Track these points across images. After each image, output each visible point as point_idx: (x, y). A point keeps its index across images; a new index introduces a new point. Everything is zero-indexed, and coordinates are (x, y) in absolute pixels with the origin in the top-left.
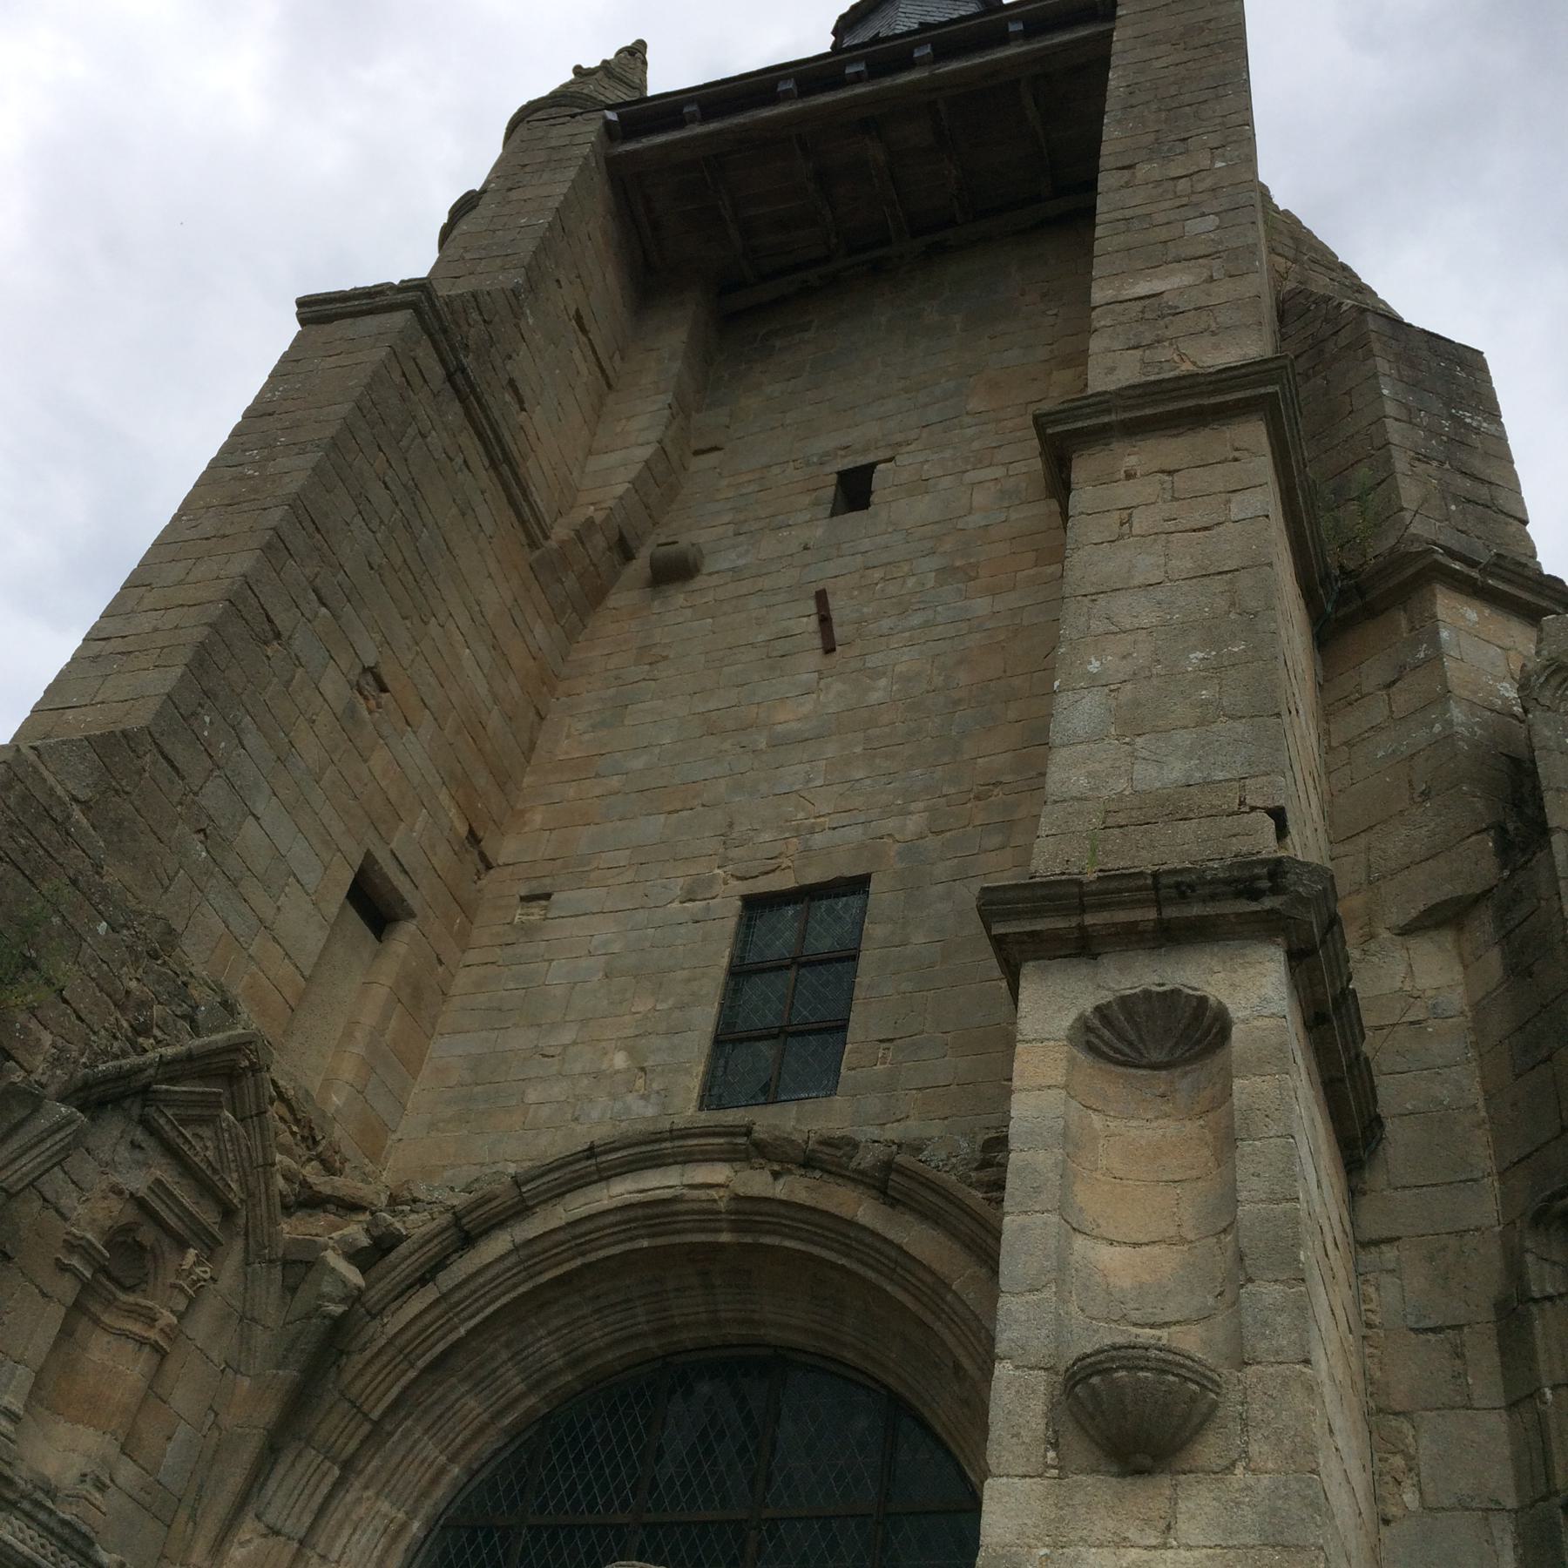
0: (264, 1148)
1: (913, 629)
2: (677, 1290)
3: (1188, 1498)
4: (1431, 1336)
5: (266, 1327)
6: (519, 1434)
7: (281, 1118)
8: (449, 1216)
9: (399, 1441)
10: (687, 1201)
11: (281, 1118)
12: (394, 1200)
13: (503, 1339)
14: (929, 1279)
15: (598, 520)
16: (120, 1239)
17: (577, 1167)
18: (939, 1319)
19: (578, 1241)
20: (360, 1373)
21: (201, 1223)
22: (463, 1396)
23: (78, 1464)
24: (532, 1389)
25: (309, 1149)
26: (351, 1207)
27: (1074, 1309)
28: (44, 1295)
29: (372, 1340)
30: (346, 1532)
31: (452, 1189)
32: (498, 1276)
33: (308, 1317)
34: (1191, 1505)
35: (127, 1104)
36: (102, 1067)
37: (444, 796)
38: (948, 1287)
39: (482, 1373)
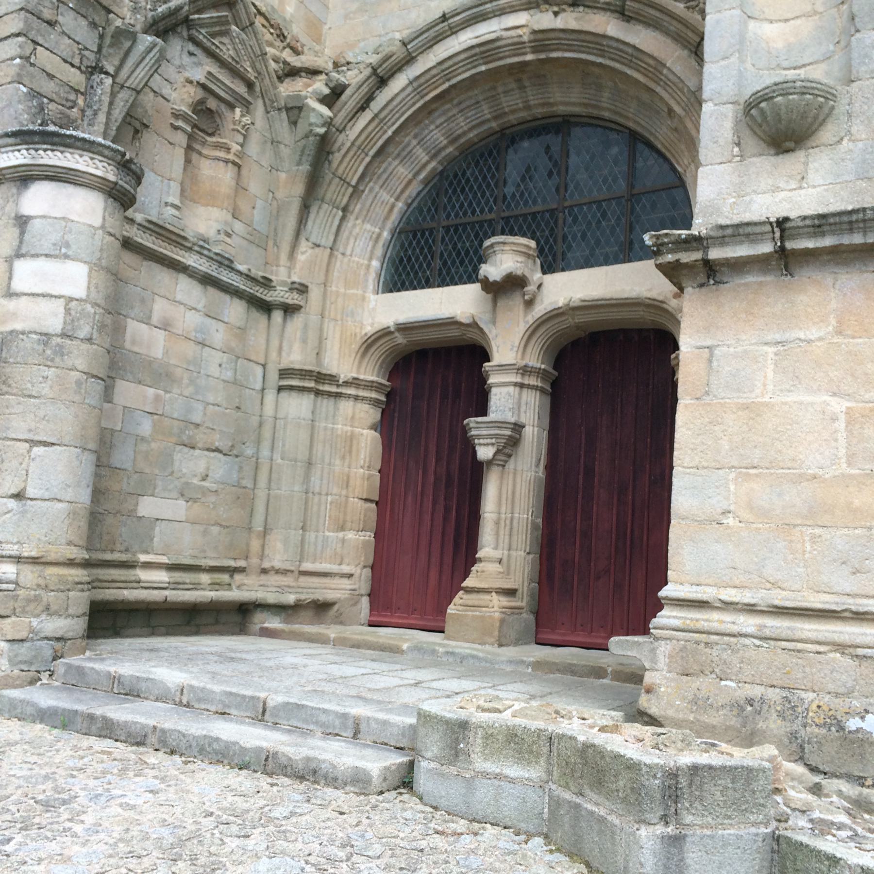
0: (259, 45)
2: (505, 92)
3: (815, 161)
5: (286, 145)
6: (429, 183)
7: (263, 25)
8: (369, 70)
9: (368, 195)
10: (505, 39)
11: (263, 25)
12: (336, 65)
13: (412, 134)
14: (651, 62)
16: (199, 108)
17: (437, 28)
18: (659, 85)
19: (445, 73)
20: (341, 162)
21: (237, 93)
22: (396, 167)
23: (216, 226)
24: (433, 157)
25: (282, 41)
26: (314, 72)
27: (749, 66)
28: (171, 144)
29: (343, 144)
30: (352, 241)
31: (367, 53)
32: (404, 99)
33: (307, 136)
34: (816, 164)
35: (179, 29)
36: (160, 10)
38: (664, 65)
39: (404, 153)
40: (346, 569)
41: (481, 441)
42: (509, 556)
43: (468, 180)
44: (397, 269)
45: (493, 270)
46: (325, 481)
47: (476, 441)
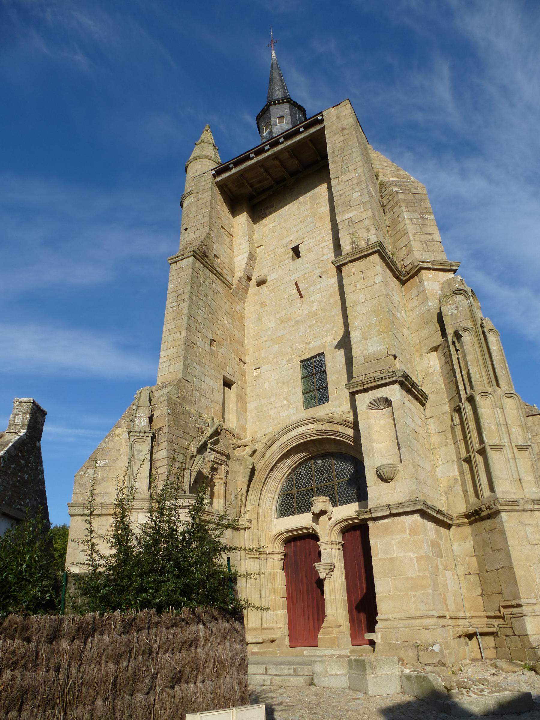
1: (318, 289)
4: (440, 433)
8: (265, 444)
15: (242, 276)
30: (265, 501)
37: (232, 355)
40: (279, 625)
41: (321, 571)
42: (337, 613)
43: (302, 475)
44: (282, 509)
45: (316, 509)
46: (267, 592)
47: (319, 571)
